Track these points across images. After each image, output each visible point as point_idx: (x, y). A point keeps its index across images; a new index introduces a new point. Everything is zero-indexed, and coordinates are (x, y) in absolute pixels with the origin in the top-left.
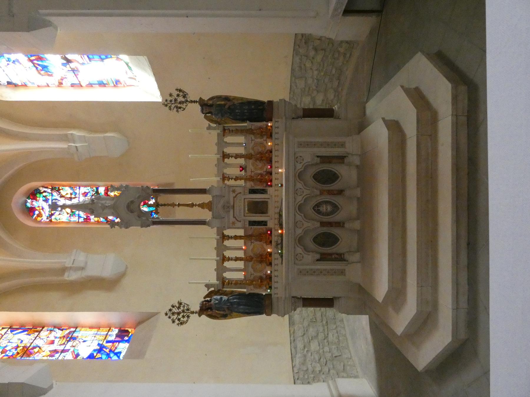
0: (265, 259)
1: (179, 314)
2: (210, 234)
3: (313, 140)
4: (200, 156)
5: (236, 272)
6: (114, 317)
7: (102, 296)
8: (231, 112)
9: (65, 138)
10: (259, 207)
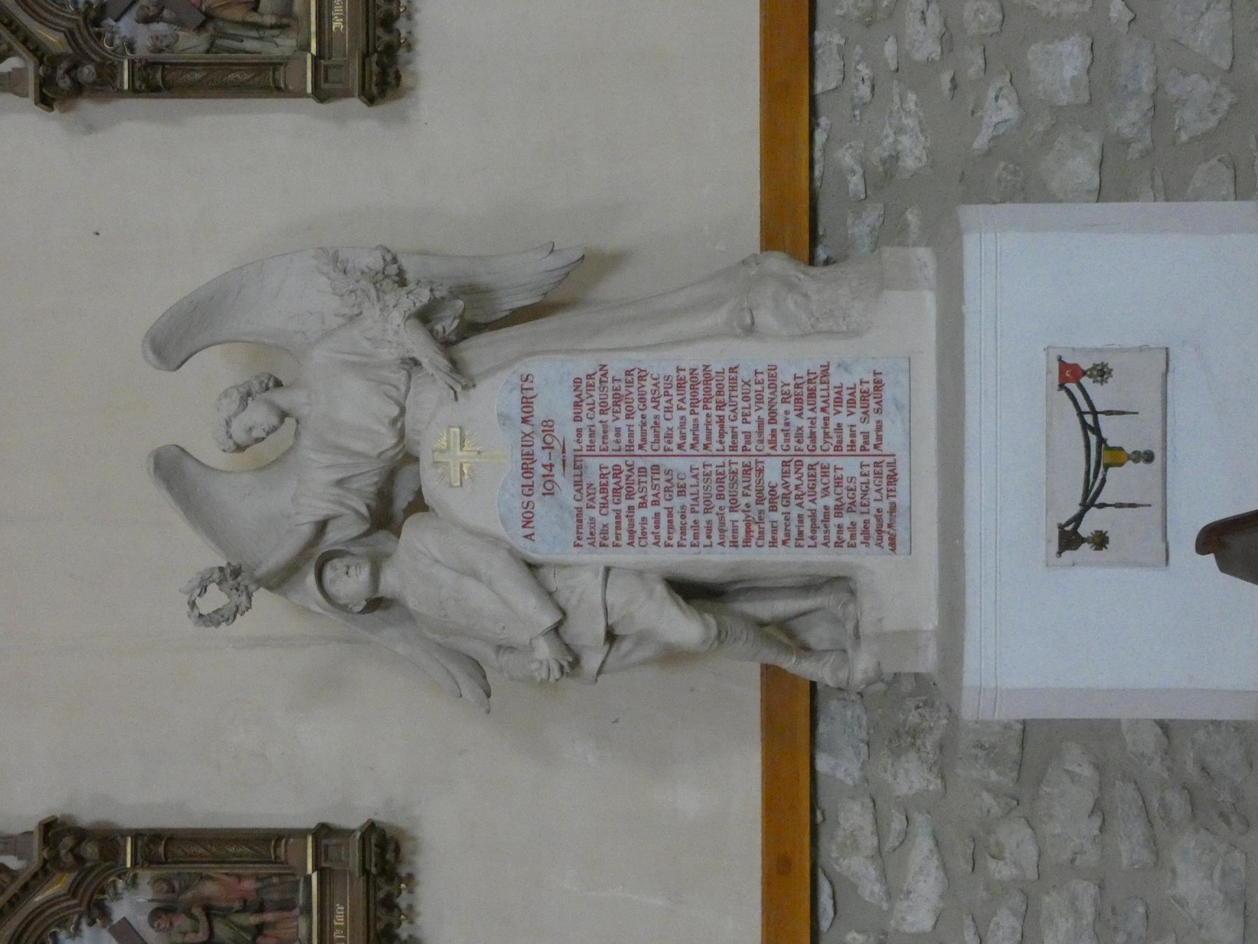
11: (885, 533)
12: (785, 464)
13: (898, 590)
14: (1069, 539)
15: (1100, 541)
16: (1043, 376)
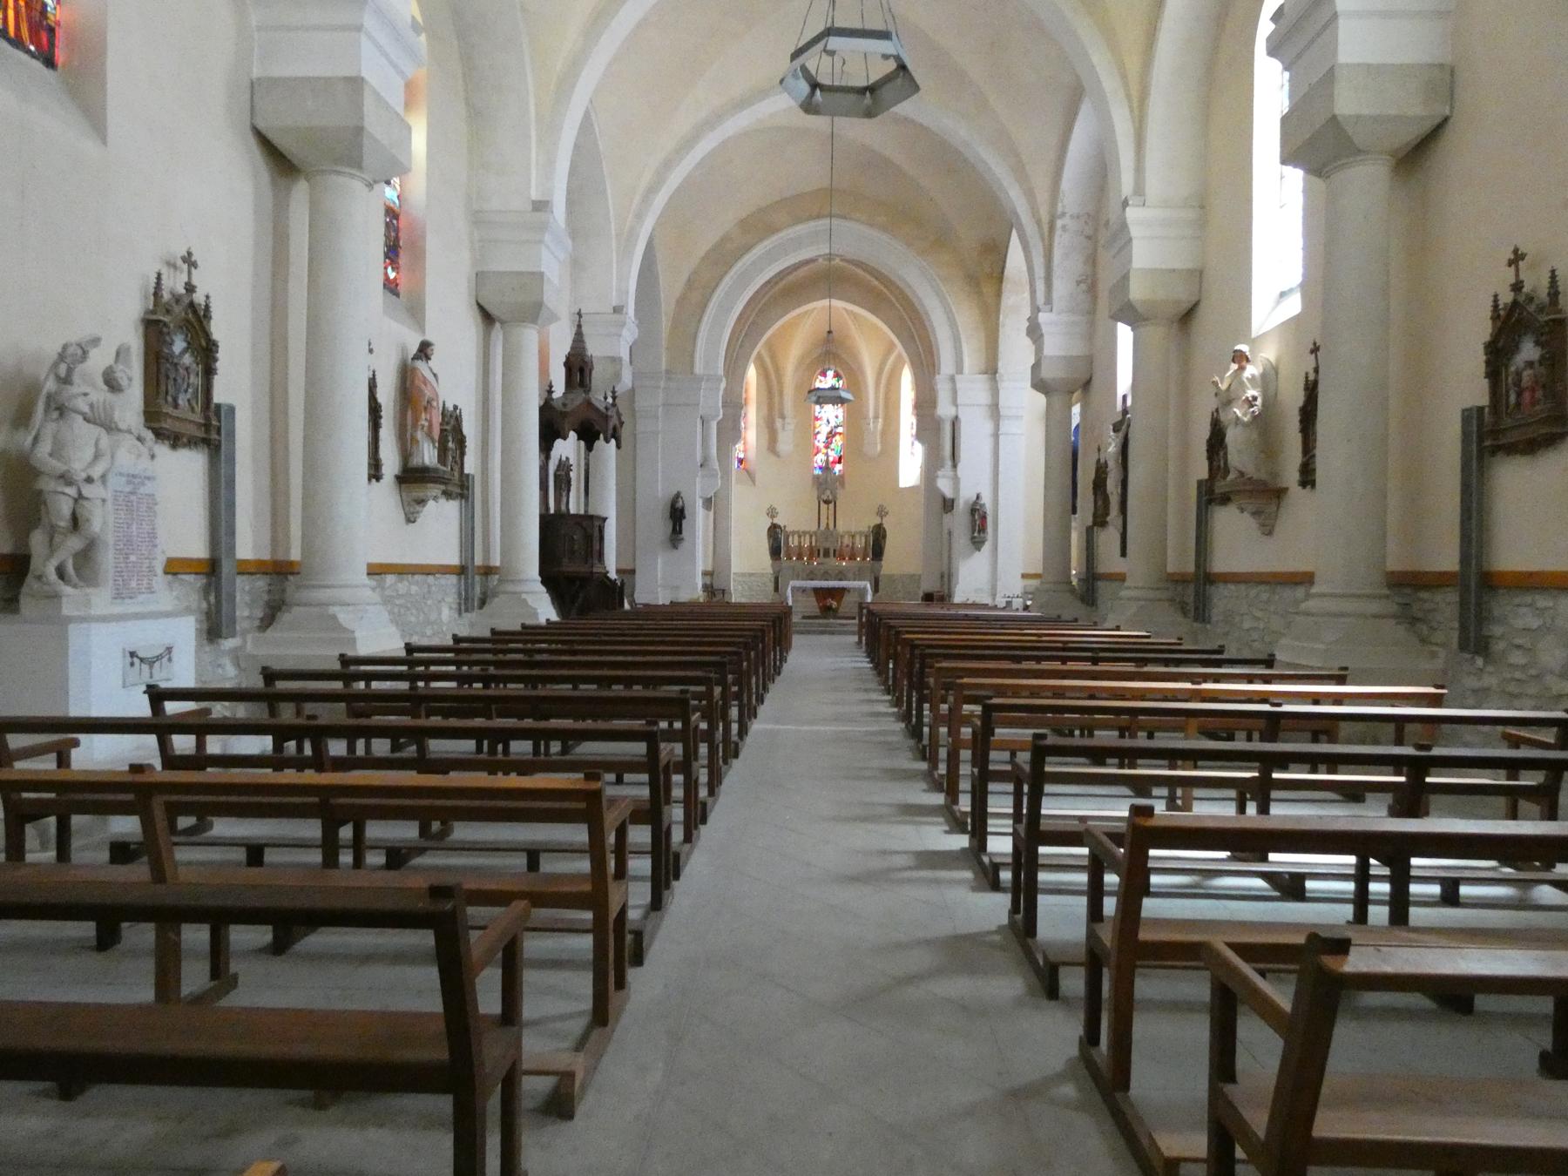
0: (852, 558)
1: (772, 513)
2: (814, 528)
3: (699, 437)
4: (854, 522)
5: (794, 542)
6: (752, 454)
7: (765, 443)
8: (878, 538)
9: (876, 417)
10: (827, 554)
11: (118, 596)
12: (1096, 868)
13: (101, 600)
14: (132, 654)
15: (132, 664)
16: (168, 642)
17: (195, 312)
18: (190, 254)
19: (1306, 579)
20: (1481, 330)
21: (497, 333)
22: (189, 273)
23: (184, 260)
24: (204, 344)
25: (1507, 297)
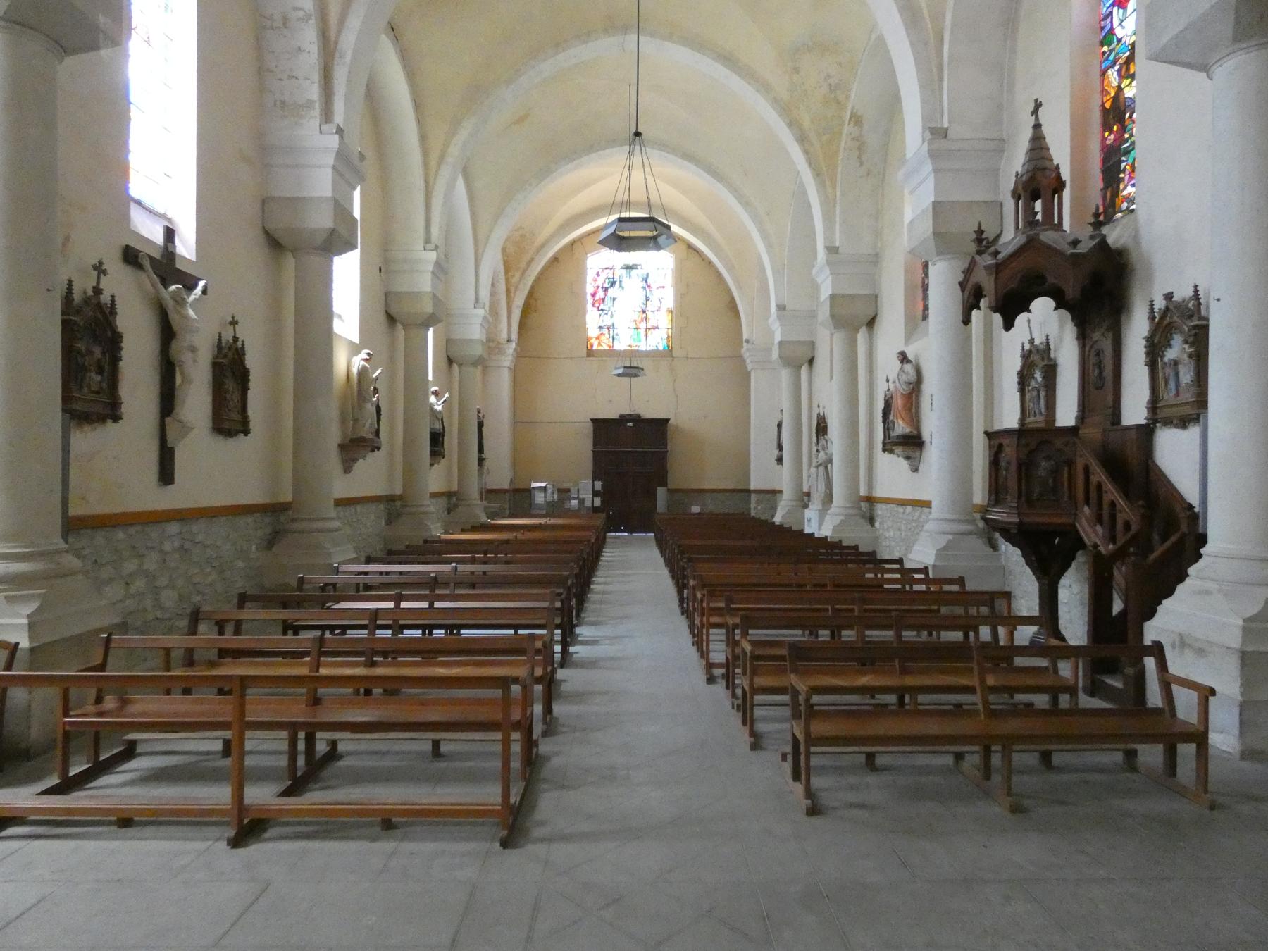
17: (103, 313)
18: (101, 263)
19: (927, 504)
20: (1017, 364)
21: (400, 332)
22: (99, 278)
23: (95, 268)
24: (109, 334)
25: (1027, 347)
